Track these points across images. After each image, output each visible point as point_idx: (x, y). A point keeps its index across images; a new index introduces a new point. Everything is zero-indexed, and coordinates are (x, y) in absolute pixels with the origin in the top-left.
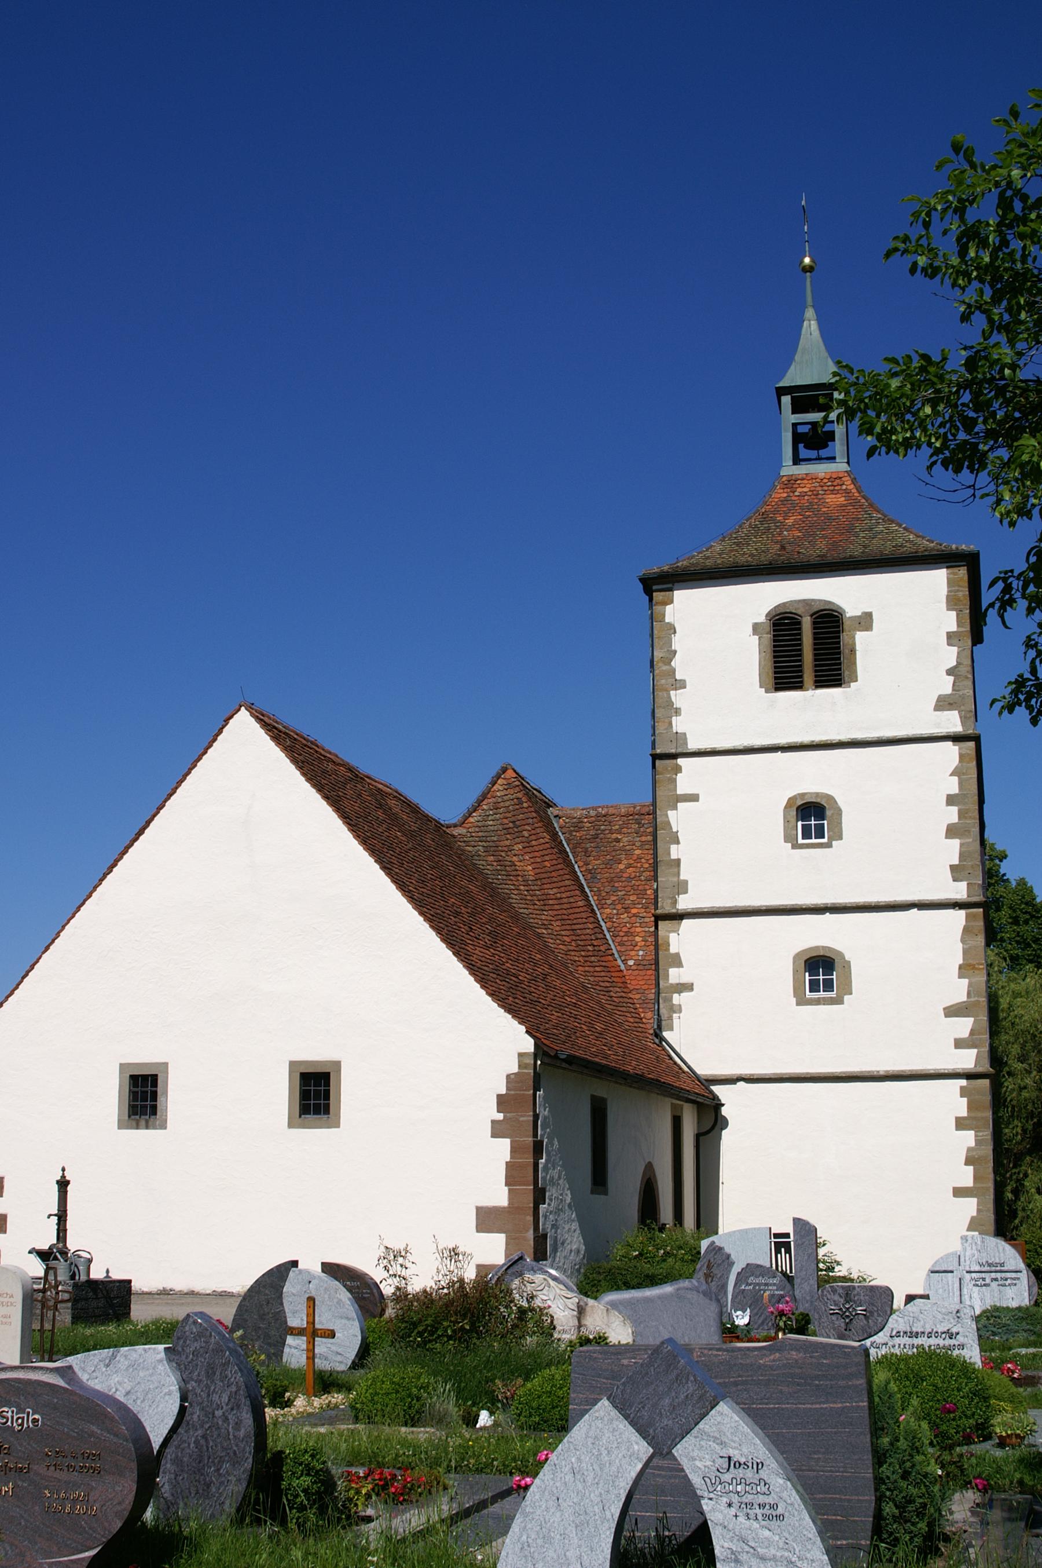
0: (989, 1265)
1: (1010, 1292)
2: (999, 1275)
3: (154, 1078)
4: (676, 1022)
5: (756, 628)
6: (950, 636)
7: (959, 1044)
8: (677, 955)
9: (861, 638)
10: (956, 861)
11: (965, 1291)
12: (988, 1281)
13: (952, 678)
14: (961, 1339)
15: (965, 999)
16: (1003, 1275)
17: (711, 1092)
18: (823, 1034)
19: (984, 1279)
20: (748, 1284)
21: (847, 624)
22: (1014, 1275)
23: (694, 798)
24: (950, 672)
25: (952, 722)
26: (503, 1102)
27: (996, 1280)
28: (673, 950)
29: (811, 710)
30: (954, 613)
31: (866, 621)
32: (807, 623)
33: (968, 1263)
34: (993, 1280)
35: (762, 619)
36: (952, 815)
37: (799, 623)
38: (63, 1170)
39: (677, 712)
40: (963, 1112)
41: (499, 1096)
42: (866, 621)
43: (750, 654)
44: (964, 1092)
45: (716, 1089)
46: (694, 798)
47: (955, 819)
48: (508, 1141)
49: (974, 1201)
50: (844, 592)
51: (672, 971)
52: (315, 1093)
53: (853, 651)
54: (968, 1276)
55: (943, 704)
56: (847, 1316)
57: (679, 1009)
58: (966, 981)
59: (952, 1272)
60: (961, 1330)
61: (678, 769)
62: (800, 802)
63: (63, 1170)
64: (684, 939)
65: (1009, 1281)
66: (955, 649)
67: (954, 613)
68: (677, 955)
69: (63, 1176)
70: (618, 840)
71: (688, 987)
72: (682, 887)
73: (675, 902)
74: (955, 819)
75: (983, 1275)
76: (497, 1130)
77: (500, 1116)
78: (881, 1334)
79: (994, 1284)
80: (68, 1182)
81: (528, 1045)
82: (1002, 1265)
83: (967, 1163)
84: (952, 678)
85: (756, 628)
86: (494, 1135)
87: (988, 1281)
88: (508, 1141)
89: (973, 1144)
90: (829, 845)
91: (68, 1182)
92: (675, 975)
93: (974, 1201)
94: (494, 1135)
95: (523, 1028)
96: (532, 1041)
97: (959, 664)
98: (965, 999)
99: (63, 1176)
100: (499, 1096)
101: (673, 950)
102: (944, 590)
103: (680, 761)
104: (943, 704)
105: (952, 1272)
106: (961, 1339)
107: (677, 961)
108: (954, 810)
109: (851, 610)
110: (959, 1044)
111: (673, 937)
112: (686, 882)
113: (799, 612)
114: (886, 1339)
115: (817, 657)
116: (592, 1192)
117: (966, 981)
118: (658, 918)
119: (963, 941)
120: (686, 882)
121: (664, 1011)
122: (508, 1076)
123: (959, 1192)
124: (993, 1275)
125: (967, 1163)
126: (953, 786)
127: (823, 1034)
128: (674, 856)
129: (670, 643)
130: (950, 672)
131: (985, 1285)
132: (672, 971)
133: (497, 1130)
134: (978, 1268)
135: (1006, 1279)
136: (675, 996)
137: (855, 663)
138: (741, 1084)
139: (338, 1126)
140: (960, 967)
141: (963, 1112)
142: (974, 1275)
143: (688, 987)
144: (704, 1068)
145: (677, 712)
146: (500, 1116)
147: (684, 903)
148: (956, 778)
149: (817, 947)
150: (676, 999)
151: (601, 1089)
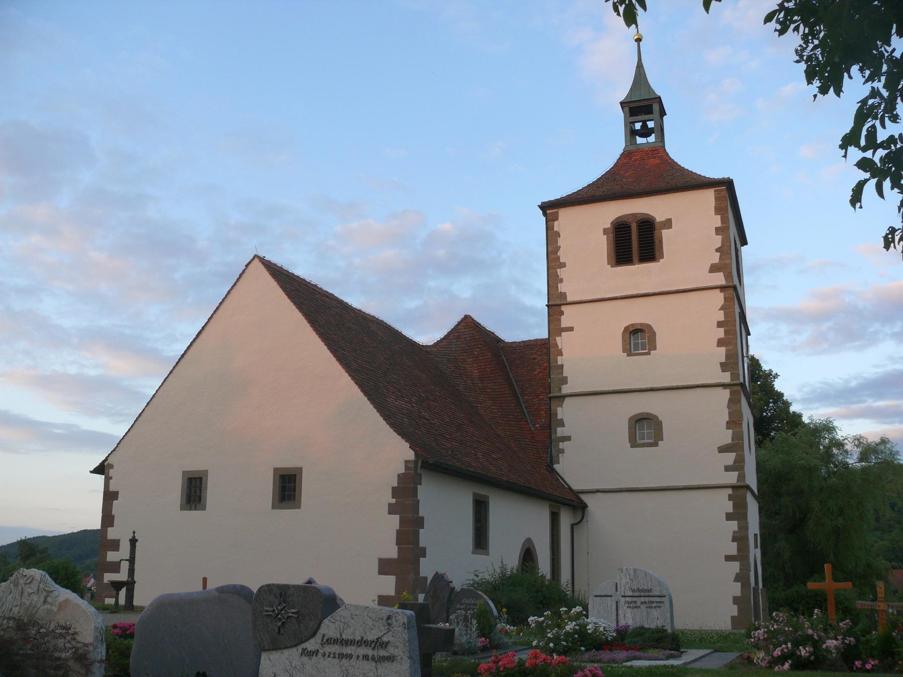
0: (639, 590)
1: (655, 613)
2: (647, 599)
3: (201, 479)
4: (561, 458)
5: (605, 231)
6: (717, 229)
7: (728, 469)
8: (562, 420)
9: (665, 232)
10: (724, 360)
11: (620, 612)
12: (638, 604)
13: (718, 254)
14: (391, 650)
15: (730, 441)
16: (651, 599)
17: (580, 499)
18: (646, 466)
19: (635, 602)
20: (462, 604)
21: (657, 226)
22: (658, 599)
23: (571, 329)
24: (717, 250)
25: (719, 279)
26: (395, 492)
27: (645, 602)
28: (559, 417)
29: (639, 276)
30: (719, 216)
31: (668, 224)
32: (634, 227)
33: (623, 589)
34: (642, 603)
35: (609, 226)
36: (721, 333)
37: (630, 227)
38: (134, 533)
39: (561, 281)
40: (730, 510)
41: (393, 488)
42: (668, 224)
43: (602, 245)
44: (730, 497)
45: (585, 498)
46: (571, 329)
47: (722, 335)
48: (398, 516)
49: (738, 563)
50: (653, 207)
51: (559, 430)
52: (287, 488)
53: (661, 242)
54: (623, 600)
55: (714, 269)
56: (280, 619)
57: (562, 451)
58: (731, 431)
59: (611, 596)
60: (391, 639)
61: (562, 313)
62: (631, 329)
63: (134, 533)
64: (566, 411)
65: (655, 604)
66: (720, 237)
67: (719, 216)
68: (562, 420)
69: (134, 537)
70: (535, 359)
71: (568, 438)
72: (565, 381)
73: (560, 390)
74: (722, 335)
75: (635, 599)
76: (392, 510)
77: (394, 501)
78: (312, 641)
79: (643, 607)
80: (137, 540)
81: (411, 455)
82: (649, 591)
83: (733, 541)
84: (718, 254)
85: (605, 231)
86: (390, 513)
87: (638, 604)
88: (398, 516)
89: (736, 529)
90: (648, 354)
91: (137, 540)
92: (560, 432)
93: (738, 563)
94: (390, 513)
95: (408, 445)
96: (413, 453)
97: (723, 245)
98: (730, 441)
99: (134, 537)
100: (393, 488)
101: (559, 417)
102: (712, 204)
103: (563, 308)
104: (714, 269)
105: (611, 596)
106: (391, 650)
107: (561, 423)
108: (722, 330)
109: (659, 218)
110: (728, 469)
111: (559, 409)
112: (566, 378)
113: (630, 221)
114: (318, 647)
115: (629, 240)
116: (473, 553)
117: (731, 431)
118: (550, 398)
119: (728, 407)
120: (566, 378)
121: (554, 453)
122: (399, 475)
123: (728, 558)
124: (642, 599)
125: (733, 541)
126: (721, 316)
127: (646, 466)
128: (559, 363)
129: (557, 242)
130: (717, 250)
131: (636, 607)
132: (559, 430)
133: (392, 510)
134: (630, 593)
135: (653, 602)
136: (561, 444)
137: (662, 248)
138: (598, 494)
139: (300, 508)
140: (727, 423)
141: (730, 510)
142: (627, 599)
143: (568, 438)
144: (576, 487)
145: (561, 281)
146: (394, 501)
147: (566, 390)
148: (722, 312)
149: (642, 414)
150: (561, 445)
151: (483, 491)
